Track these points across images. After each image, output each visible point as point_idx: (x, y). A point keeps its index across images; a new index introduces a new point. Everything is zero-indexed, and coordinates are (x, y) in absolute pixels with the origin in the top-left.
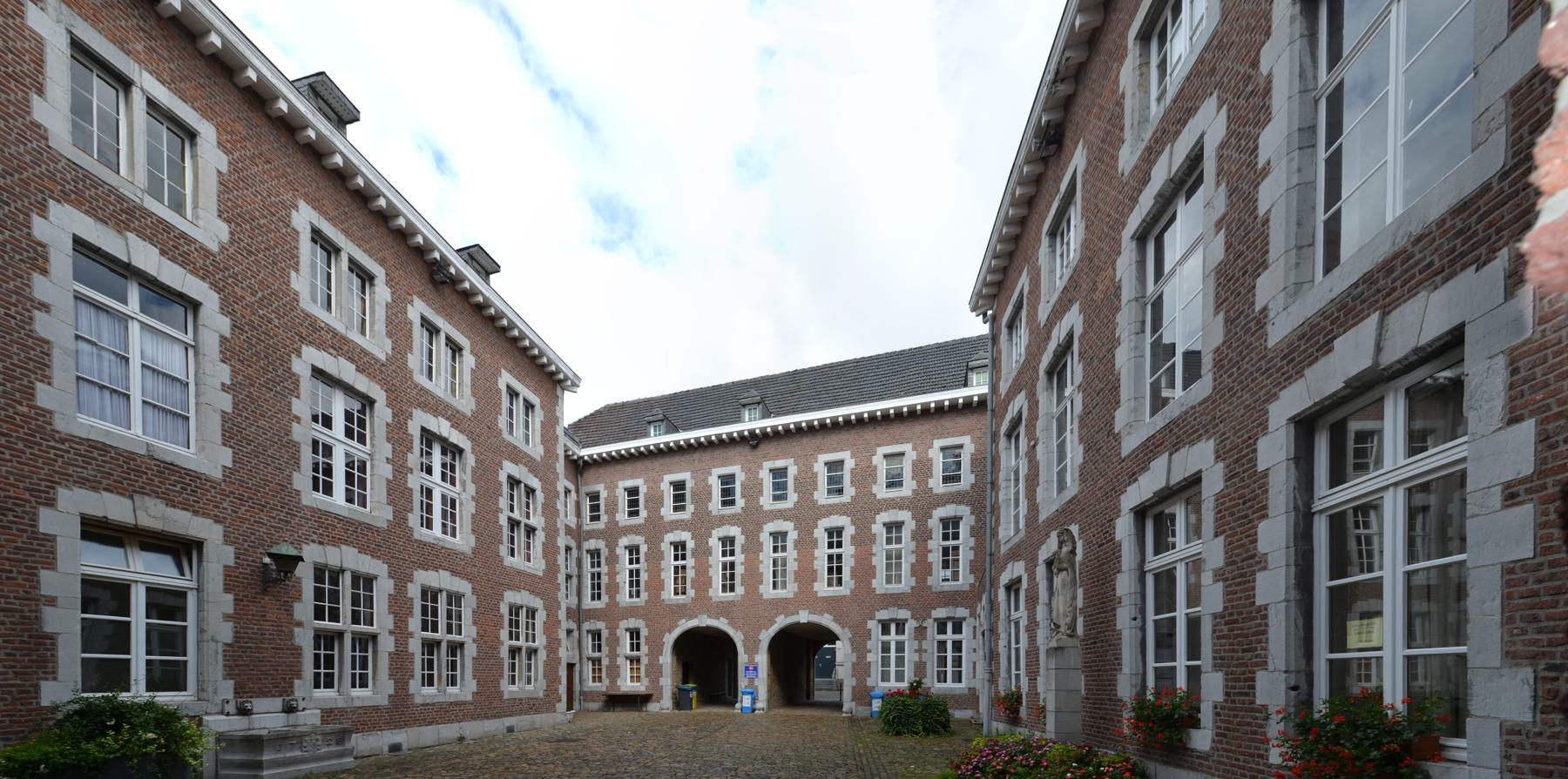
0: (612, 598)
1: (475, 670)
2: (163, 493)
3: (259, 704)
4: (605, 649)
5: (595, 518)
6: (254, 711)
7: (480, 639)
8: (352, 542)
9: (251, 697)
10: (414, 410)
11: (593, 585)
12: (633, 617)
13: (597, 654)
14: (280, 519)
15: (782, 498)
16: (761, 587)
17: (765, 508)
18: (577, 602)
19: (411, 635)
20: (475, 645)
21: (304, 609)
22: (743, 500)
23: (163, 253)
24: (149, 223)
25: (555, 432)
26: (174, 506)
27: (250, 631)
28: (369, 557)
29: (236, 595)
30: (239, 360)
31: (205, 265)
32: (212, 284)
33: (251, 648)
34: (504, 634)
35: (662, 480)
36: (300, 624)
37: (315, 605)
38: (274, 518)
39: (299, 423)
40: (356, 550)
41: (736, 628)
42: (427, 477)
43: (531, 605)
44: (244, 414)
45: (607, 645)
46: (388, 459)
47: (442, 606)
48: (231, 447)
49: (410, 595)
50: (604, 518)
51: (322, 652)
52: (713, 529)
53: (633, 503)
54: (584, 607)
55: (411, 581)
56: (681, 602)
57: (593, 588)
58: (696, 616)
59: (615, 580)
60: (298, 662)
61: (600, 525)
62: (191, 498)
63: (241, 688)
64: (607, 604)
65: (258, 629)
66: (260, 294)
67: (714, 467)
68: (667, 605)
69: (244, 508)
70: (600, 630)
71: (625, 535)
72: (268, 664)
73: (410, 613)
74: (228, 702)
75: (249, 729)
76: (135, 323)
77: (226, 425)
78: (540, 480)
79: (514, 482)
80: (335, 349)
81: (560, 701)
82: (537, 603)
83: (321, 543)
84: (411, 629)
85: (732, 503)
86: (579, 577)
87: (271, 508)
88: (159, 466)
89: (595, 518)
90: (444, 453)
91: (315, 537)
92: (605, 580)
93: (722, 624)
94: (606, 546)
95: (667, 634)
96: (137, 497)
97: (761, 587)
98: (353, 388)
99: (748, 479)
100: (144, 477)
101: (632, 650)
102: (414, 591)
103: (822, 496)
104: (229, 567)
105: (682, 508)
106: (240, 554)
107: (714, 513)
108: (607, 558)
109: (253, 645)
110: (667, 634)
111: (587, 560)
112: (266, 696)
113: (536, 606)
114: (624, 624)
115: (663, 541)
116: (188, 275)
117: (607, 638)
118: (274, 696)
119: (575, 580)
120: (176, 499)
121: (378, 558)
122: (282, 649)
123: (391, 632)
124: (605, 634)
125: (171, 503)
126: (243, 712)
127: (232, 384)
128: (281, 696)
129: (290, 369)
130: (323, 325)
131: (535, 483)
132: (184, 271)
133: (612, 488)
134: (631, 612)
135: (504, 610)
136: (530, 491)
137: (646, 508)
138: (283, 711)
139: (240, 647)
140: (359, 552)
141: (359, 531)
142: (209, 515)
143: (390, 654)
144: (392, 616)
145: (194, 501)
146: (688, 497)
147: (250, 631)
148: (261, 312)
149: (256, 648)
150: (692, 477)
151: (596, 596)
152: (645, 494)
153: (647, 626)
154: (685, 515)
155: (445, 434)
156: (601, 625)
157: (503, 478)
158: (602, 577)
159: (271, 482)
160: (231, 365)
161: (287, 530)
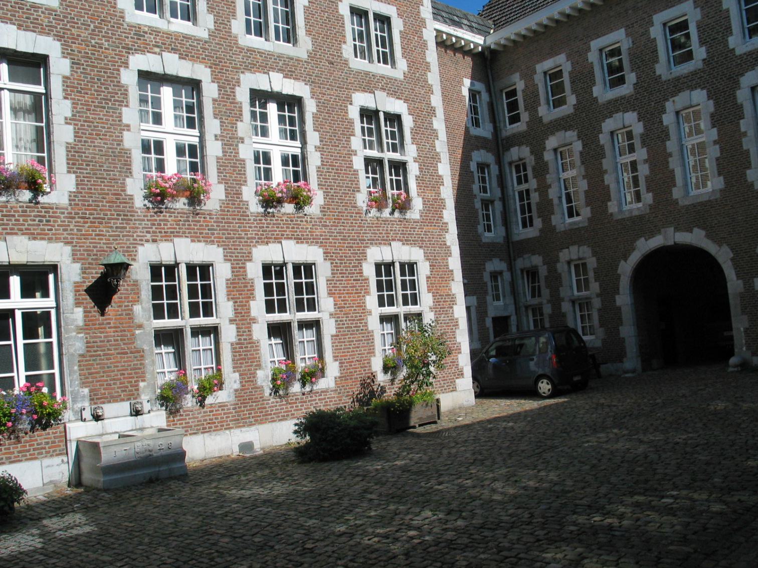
0: (546, 220)
1: (336, 349)
2: (26, 229)
3: (108, 409)
4: (546, 292)
5: (515, 119)
6: (106, 416)
7: (340, 312)
8: (184, 233)
9: (104, 403)
10: (242, 75)
11: (522, 207)
12: (574, 244)
13: (536, 301)
14: (117, 227)
15: (559, 103)
16: (748, 172)
17: (738, 52)
18: (504, 234)
19: (254, 321)
20: (333, 320)
21: (142, 309)
22: (704, 49)
23: (20, 27)
24: (10, 8)
25: (421, 37)
26: (35, 239)
27: (98, 340)
28: (203, 244)
29: (85, 307)
30: (78, 92)
31: (49, 22)
32: (55, 35)
33: (100, 355)
34: (372, 301)
35: (589, 49)
36: (140, 326)
37: (153, 304)
38: (111, 227)
39: (129, 130)
40: (189, 240)
41: (719, 242)
42: (263, 140)
43: (405, 258)
44: (83, 139)
45: (547, 287)
46: (216, 136)
47: (290, 280)
48: (74, 172)
49: (250, 276)
50: (525, 117)
51: (409, 292)
52: (667, 100)
53: (558, 89)
54: (516, 238)
55: (250, 260)
56: (636, 213)
57: (523, 212)
58: (659, 232)
59: (547, 195)
60: (141, 364)
61: (520, 127)
62: (46, 228)
63: (95, 395)
64: (541, 231)
65: (105, 337)
66: (92, 26)
67: (656, 12)
68: (617, 221)
69: (87, 225)
70: (536, 267)
71: (553, 133)
72: (116, 369)
73: (251, 296)
74: (84, 409)
75: (102, 435)
76: (6, 91)
77: (70, 154)
78: (406, 101)
79: (368, 115)
80: (158, 47)
81: (461, 375)
82: (414, 254)
83: (154, 241)
84: (254, 313)
85: (689, 56)
86: (504, 199)
87: (109, 219)
88: (23, 207)
89: (515, 119)
90: (281, 108)
91: (149, 236)
92: (535, 197)
93: (696, 238)
94: (532, 153)
95: (622, 262)
96: (8, 238)
97: (748, 172)
98: (177, 77)
99: (705, 16)
100: (13, 219)
101: (579, 290)
102: (254, 271)
103: (664, 69)
104: (78, 282)
105: (621, 81)
106: (86, 269)
107: (664, 78)
108: (534, 169)
109: (101, 353)
110: (622, 262)
111: (512, 177)
112: (117, 401)
113: (413, 259)
114: (564, 255)
115: (600, 132)
116: (38, 36)
117: (546, 277)
118: (123, 400)
119: (498, 205)
120: (35, 232)
121: (212, 242)
122: (126, 353)
123: (231, 321)
124: (543, 271)
125: (33, 237)
126: (97, 418)
127: (73, 115)
128: (129, 399)
129: (119, 82)
130: (146, 29)
131: (397, 106)
132: (34, 34)
133: (528, 76)
134: (574, 236)
135: (369, 271)
136: (394, 119)
137: (574, 91)
138: (131, 415)
139: (91, 356)
140: (193, 241)
141: (191, 219)
142: (60, 238)
143: (232, 344)
144: (231, 303)
145: (48, 230)
146: (626, 64)
147: (98, 340)
148: (93, 41)
149: (104, 355)
150: (627, 35)
151: (527, 223)
152: (570, 73)
153: (595, 254)
154: (625, 90)
155: (277, 88)
156: (536, 260)
157: (354, 113)
158: (639, 167)
159: (108, 194)
160: (72, 99)
161: (123, 236)
